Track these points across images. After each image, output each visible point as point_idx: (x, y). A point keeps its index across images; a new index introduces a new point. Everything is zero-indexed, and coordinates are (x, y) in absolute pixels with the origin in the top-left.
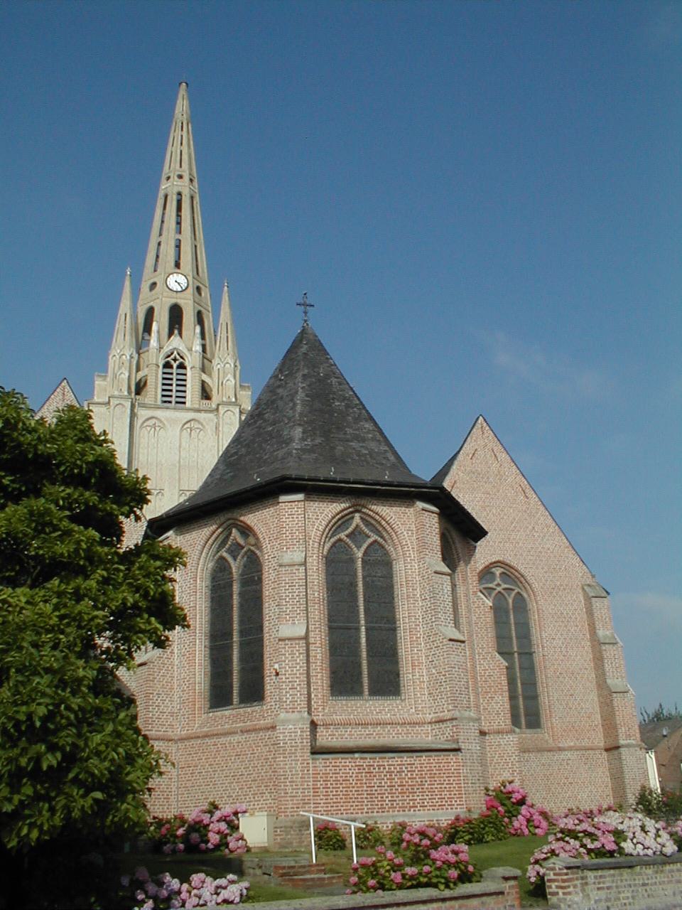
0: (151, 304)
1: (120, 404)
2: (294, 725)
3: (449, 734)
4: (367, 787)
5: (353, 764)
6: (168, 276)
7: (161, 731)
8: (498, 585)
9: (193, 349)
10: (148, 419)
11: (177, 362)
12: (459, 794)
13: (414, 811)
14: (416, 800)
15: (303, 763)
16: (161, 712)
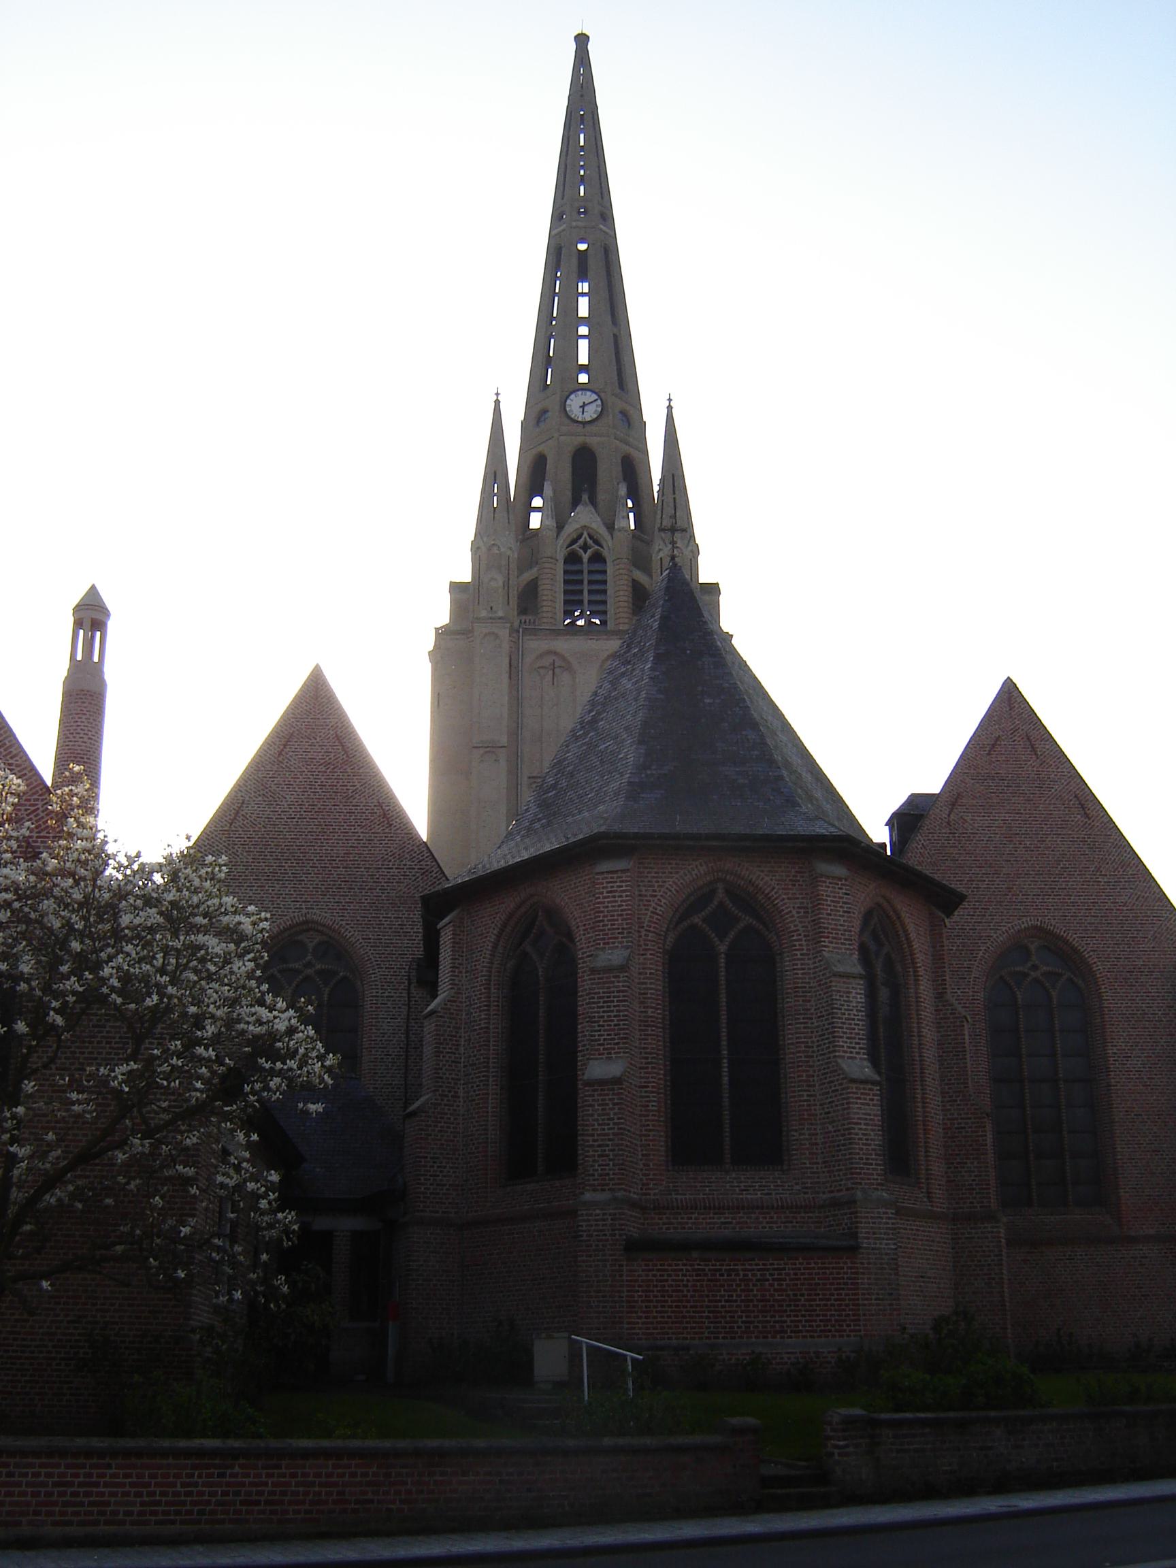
0: (540, 448)
1: (493, 633)
2: (602, 1209)
3: (846, 1224)
4: (709, 1301)
5: (689, 1268)
6: (568, 397)
7: (437, 1212)
8: (1035, 967)
9: (616, 527)
10: (541, 656)
11: (589, 552)
12: (854, 1315)
13: (781, 1338)
14: (786, 1322)
15: (615, 1265)
16: (438, 1185)
